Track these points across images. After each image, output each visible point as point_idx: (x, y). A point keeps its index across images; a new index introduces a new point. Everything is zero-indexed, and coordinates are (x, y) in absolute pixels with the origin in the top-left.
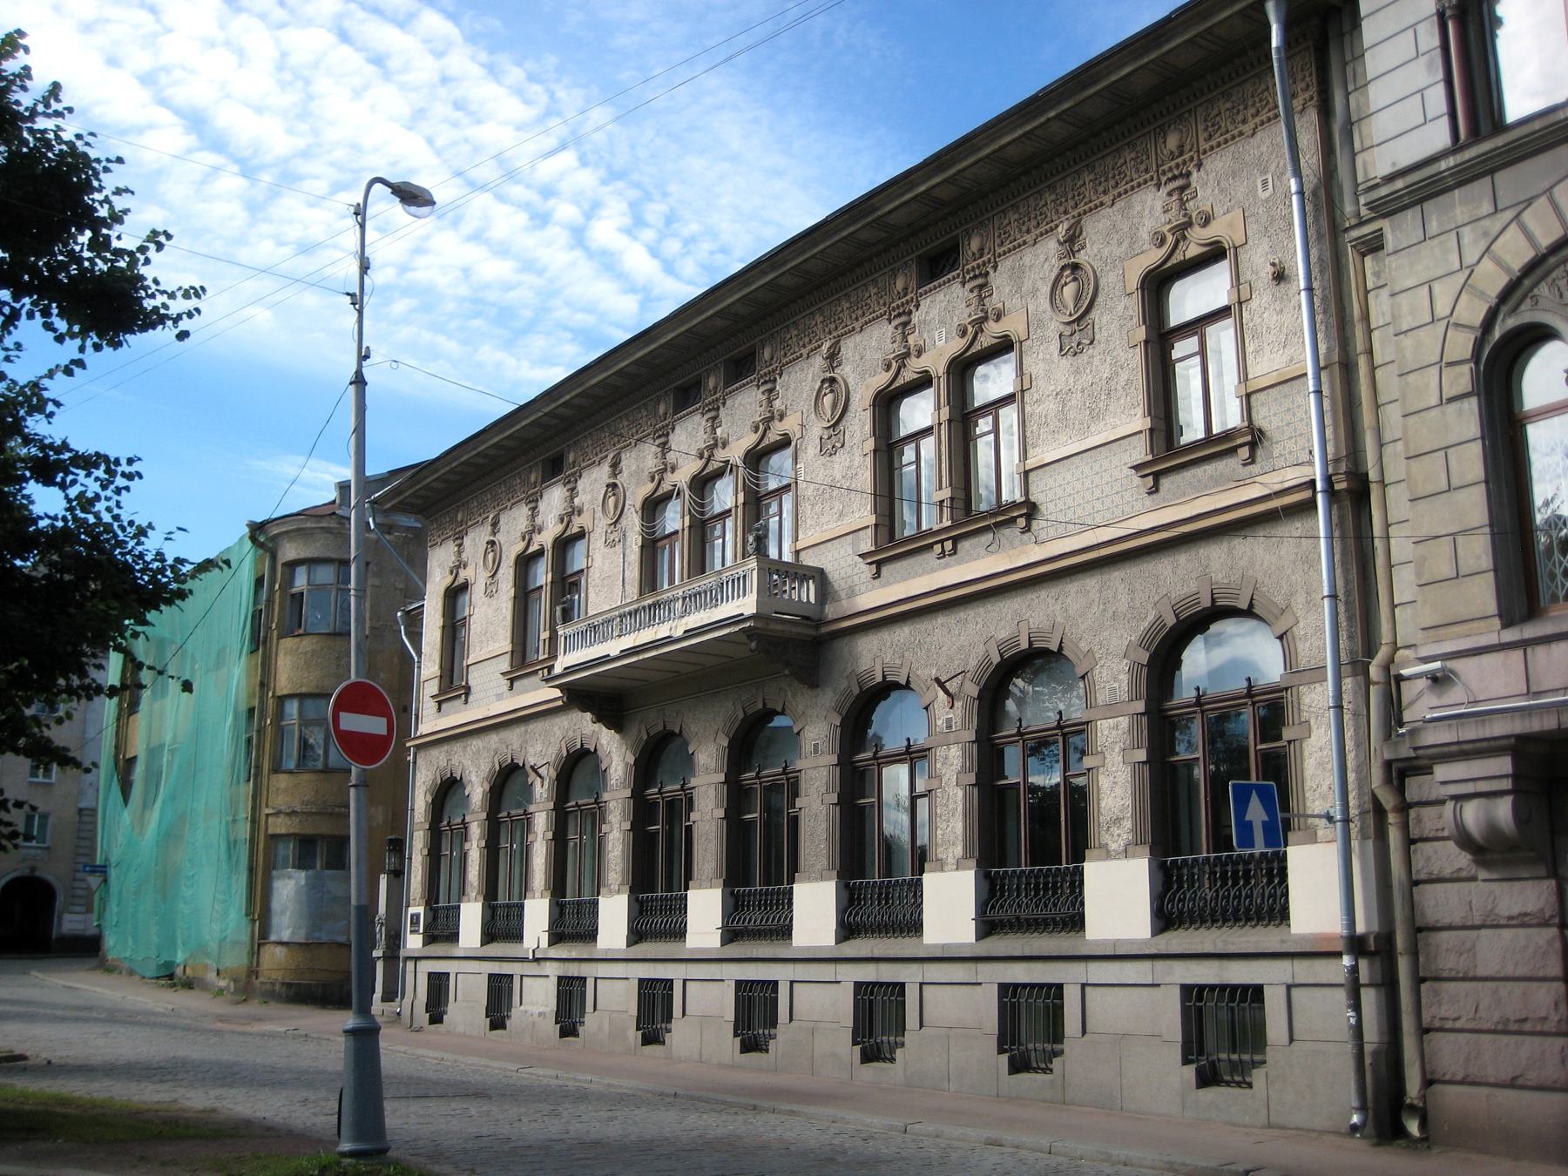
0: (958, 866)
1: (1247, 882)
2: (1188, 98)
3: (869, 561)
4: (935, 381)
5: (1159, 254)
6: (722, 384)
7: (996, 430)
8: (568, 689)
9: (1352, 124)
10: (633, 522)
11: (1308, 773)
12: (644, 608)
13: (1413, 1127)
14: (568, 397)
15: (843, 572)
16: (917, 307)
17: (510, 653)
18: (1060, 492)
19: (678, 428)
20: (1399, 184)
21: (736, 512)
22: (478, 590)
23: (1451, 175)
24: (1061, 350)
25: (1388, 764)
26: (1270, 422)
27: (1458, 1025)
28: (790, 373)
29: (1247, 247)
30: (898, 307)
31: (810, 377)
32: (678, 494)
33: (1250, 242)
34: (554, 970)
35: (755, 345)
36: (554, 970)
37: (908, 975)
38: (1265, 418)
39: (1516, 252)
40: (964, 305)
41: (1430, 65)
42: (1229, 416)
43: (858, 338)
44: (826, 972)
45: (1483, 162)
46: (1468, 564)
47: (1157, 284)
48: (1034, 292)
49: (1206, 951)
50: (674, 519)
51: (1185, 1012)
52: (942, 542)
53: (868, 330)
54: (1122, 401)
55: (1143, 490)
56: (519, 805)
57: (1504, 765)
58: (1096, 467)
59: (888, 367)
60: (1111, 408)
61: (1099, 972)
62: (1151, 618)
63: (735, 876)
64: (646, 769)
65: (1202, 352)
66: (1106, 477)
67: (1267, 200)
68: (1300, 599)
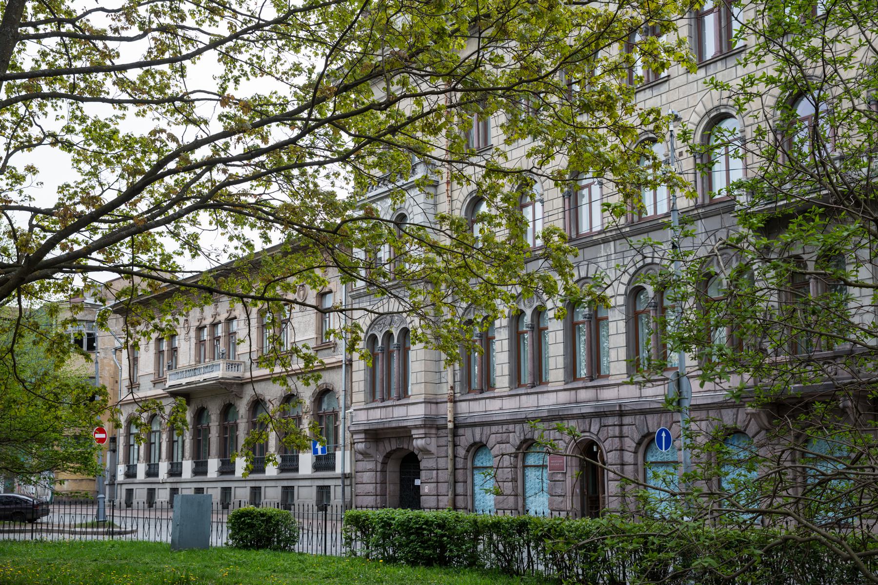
10: (193, 334)
22: (142, 348)
34: (168, 486)
36: (168, 486)
37: (262, 484)
44: (307, 483)
50: (206, 335)
61: (302, 483)
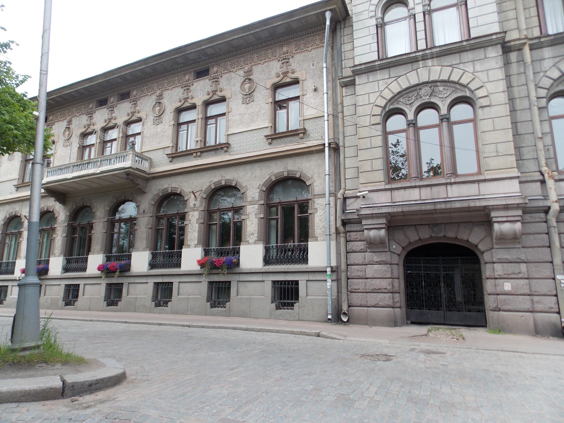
0: (196, 246)
1: (172, 258)
2: (296, 37)
3: (169, 156)
4: (197, 107)
5: (105, 124)
6: (95, 107)
7: (111, 147)
8: (47, 189)
9: (342, 52)
11: (316, 222)
12: (83, 164)
13: (345, 319)
14: (54, 96)
15: (158, 159)
16: (193, 85)
17: (18, 179)
18: (239, 141)
19: (97, 112)
20: (363, 66)
21: (119, 139)
23: (378, 66)
24: (243, 102)
25: (342, 220)
26: (310, 128)
27: (359, 291)
28: (143, 100)
29: (306, 81)
30: (111, 106)
31: (151, 101)
32: (95, 133)
33: (307, 80)
35: (130, 90)
38: (308, 127)
39: (396, 89)
40: (210, 86)
41: (373, 38)
42: (222, 139)
43: (170, 92)
44: (144, 280)
45: (388, 64)
46: (376, 168)
47: (179, 111)
48: (234, 85)
49: (281, 271)
51: (154, 288)
52: (196, 153)
53: (174, 90)
54: (262, 118)
55: (168, 161)
56: (16, 228)
57: (384, 221)
58: (252, 135)
59: (85, 127)
60: (258, 119)
62: (267, 178)
63: (68, 252)
64: (74, 216)
65: (216, 123)
66: (255, 138)
67: (313, 69)
68: (316, 175)
